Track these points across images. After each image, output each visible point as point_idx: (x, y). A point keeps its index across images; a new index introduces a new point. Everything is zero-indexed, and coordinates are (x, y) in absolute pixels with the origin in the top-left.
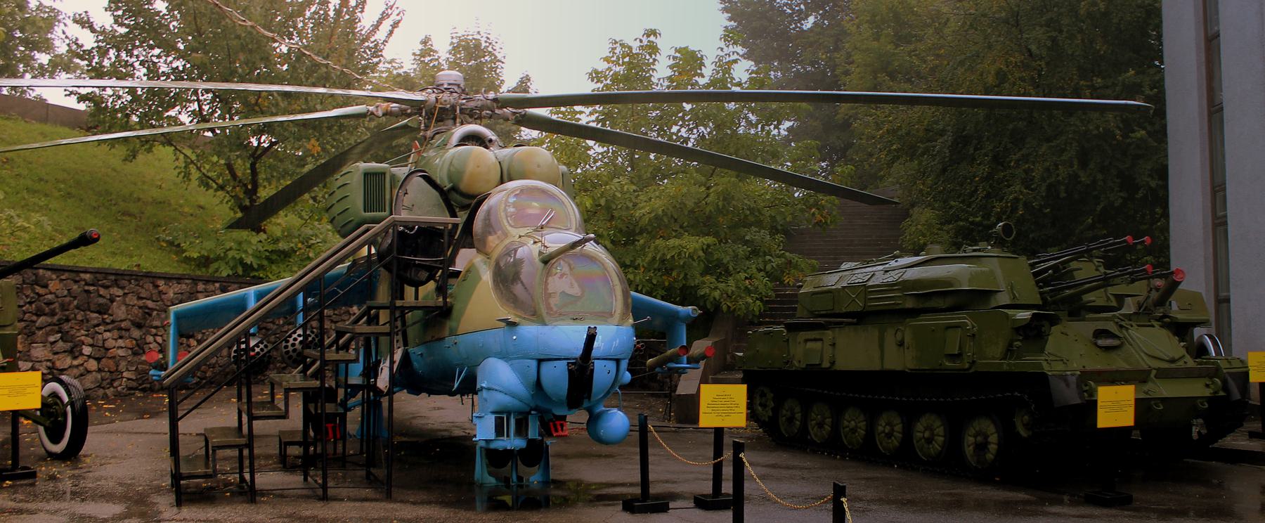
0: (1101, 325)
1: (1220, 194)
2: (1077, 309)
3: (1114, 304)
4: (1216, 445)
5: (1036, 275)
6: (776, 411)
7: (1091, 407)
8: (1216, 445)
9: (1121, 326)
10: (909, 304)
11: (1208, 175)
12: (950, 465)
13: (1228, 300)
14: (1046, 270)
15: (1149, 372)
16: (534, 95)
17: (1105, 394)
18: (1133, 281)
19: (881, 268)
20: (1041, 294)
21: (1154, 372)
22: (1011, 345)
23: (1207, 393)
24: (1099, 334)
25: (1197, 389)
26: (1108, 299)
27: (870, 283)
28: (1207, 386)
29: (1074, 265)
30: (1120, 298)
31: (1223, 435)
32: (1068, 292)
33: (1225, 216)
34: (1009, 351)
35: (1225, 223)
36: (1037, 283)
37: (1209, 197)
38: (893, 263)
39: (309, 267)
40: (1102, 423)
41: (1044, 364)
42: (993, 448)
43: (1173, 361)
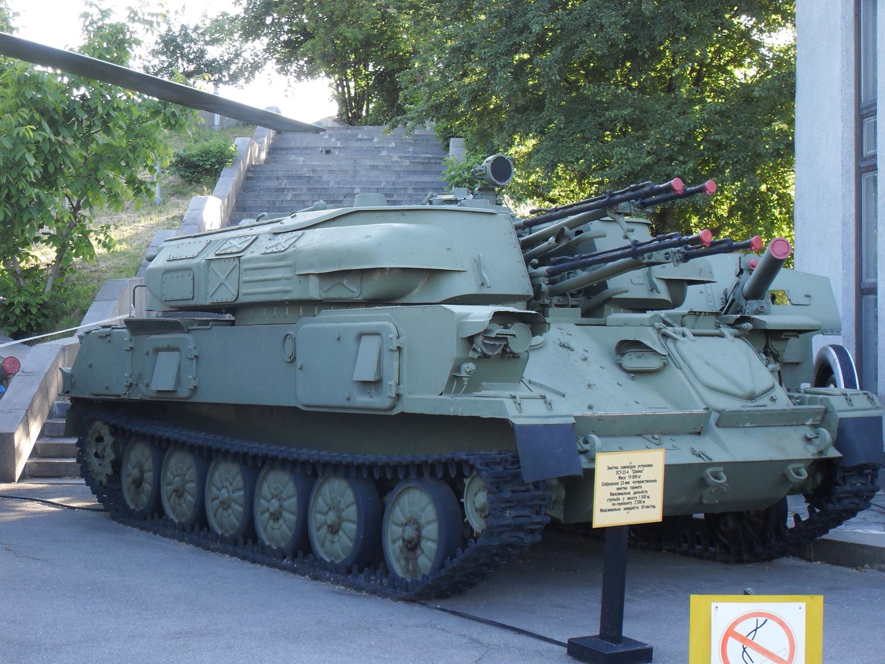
0: (629, 334)
1: (867, 121)
2: (593, 303)
3: (663, 294)
4: (825, 537)
5: (525, 246)
6: (117, 465)
7: (581, 485)
8: (825, 537)
9: (665, 336)
10: (314, 290)
11: (852, 91)
12: (366, 567)
13: (873, 290)
14: (544, 238)
15: (707, 416)
16: (197, 89)
17: (607, 466)
18: (686, 258)
19: (268, 228)
20: (532, 277)
21: (714, 416)
22: (457, 368)
23: (809, 453)
24: (626, 346)
25: (793, 447)
26: (653, 288)
27: (247, 255)
28: (808, 440)
29: (596, 226)
30: (678, 286)
31: (839, 519)
32: (582, 274)
33: (875, 156)
34: (455, 381)
35: (874, 168)
36: (527, 260)
37: (852, 125)
38: (288, 221)
39: (732, 307)
40: (600, 520)
41: (509, 404)
42: (430, 546)
43: (751, 397)
